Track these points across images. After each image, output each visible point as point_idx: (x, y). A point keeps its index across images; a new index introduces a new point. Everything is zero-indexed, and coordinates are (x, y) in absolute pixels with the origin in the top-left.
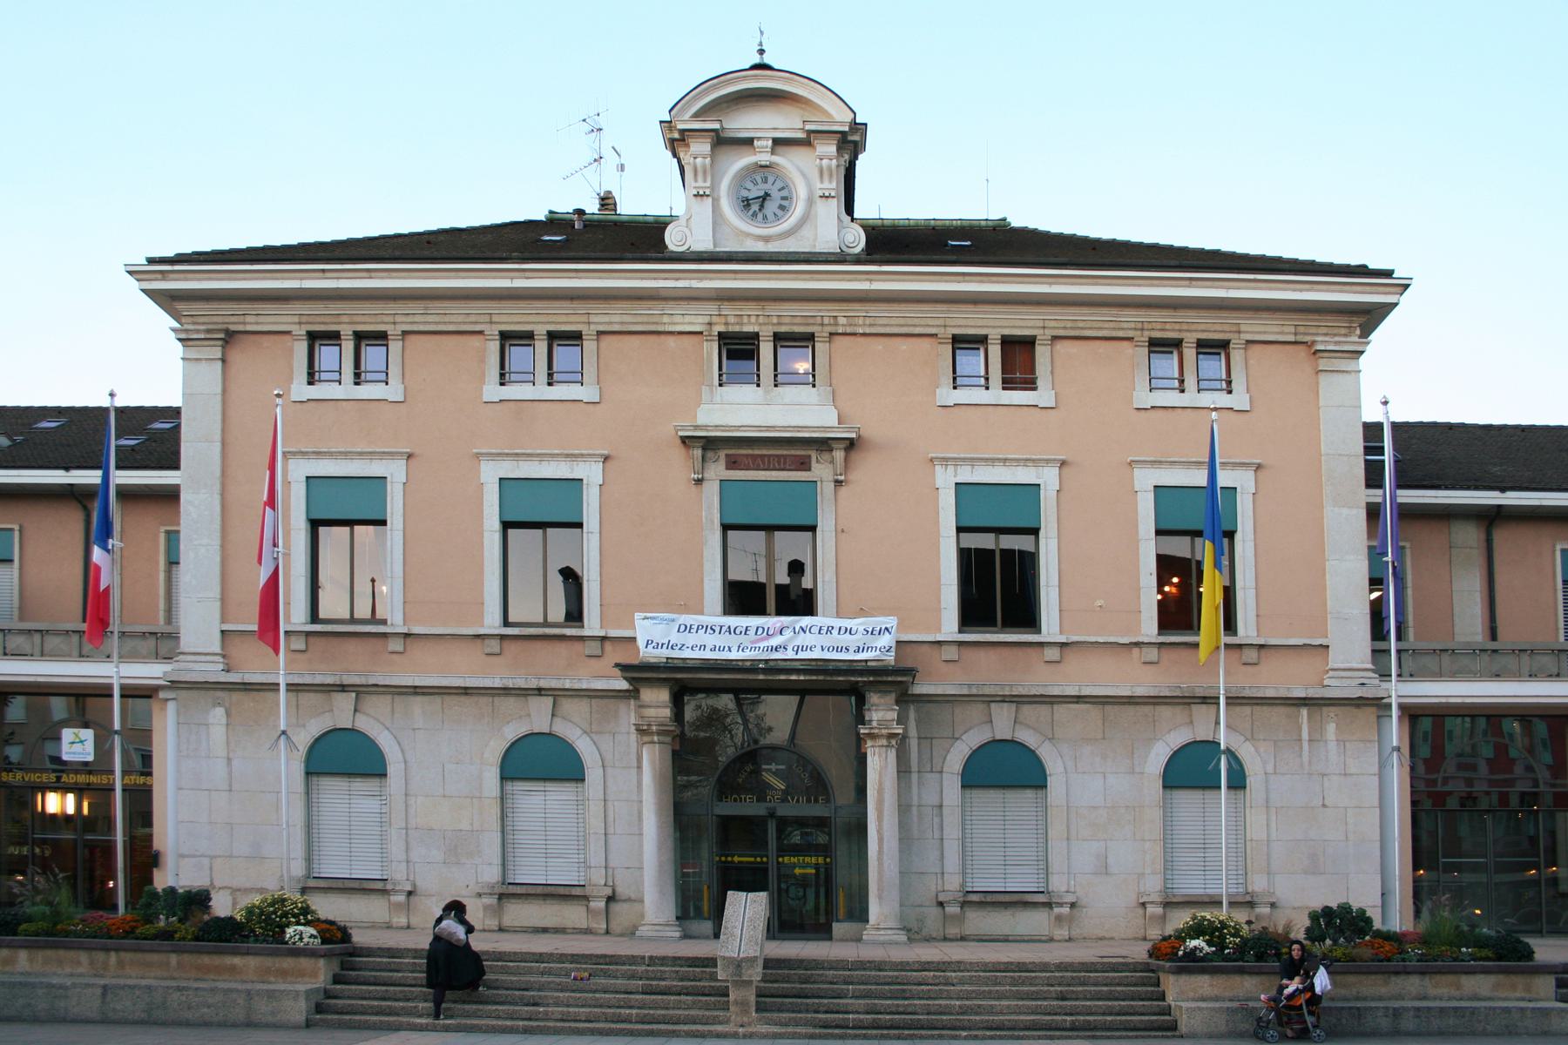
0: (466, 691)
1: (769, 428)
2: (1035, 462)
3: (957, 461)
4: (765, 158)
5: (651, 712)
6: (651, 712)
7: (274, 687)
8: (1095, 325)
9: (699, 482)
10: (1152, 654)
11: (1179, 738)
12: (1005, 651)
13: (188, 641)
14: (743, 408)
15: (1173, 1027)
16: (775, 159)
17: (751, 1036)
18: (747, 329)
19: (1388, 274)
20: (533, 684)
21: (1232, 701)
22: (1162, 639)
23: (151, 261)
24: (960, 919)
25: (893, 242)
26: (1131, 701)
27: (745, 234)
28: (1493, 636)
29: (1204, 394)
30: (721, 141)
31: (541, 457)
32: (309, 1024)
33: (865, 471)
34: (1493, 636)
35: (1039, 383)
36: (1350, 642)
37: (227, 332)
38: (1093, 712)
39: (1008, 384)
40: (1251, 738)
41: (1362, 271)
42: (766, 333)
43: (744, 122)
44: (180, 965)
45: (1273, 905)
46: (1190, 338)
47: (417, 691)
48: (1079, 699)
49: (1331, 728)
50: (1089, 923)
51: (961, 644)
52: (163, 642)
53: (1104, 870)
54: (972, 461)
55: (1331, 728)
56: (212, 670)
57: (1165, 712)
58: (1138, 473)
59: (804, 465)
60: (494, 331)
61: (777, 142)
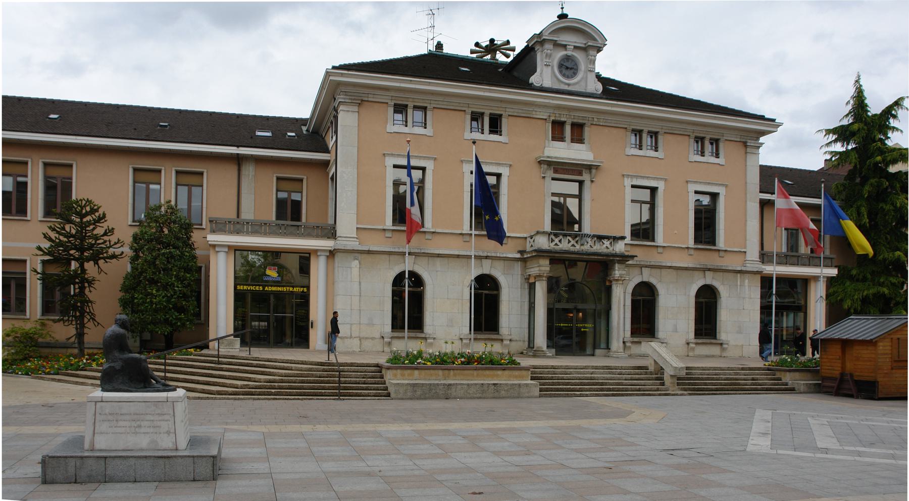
0: (458, 256)
1: (570, 159)
2: (425, 158)
3: (632, 176)
4: (569, 53)
5: (543, 268)
6: (543, 268)
7: (469, 257)
8: (677, 130)
9: (544, 177)
10: (692, 252)
11: (701, 283)
12: (645, 249)
13: (340, 231)
14: (565, 151)
15: (388, 395)
16: (574, 54)
17: (677, 395)
18: (563, 119)
19: (773, 120)
20: (485, 254)
21: (409, 254)
22: (395, 228)
23: (334, 68)
24: (693, 349)
25: (617, 90)
26: (686, 269)
27: (563, 83)
28: (238, 217)
29: (416, 128)
30: (556, 45)
31: (643, 177)
32: (541, 396)
33: (600, 178)
34: (238, 217)
35: (585, 141)
36: (753, 253)
37: (362, 101)
38: (674, 272)
39: (491, 132)
40: (723, 284)
41: (762, 118)
42: (569, 121)
43: (564, 38)
44: (478, 375)
45: (688, 344)
46: (411, 105)
47: (439, 256)
48: (670, 267)
49: (747, 281)
50: (731, 352)
51: (393, 230)
52: (331, 233)
53: (675, 330)
54: (637, 177)
55: (747, 281)
56: (354, 245)
57: (696, 273)
58: (387, 158)
59: (580, 174)
60: (469, 111)
61: (575, 47)
